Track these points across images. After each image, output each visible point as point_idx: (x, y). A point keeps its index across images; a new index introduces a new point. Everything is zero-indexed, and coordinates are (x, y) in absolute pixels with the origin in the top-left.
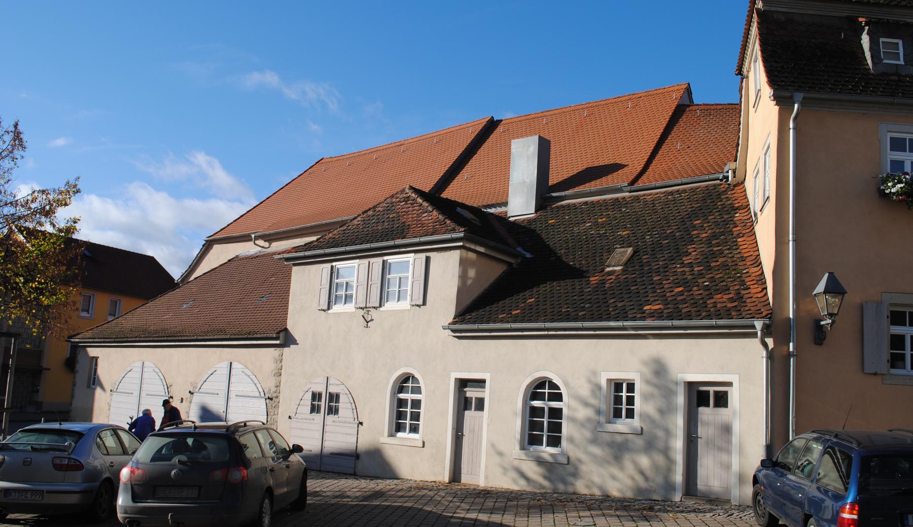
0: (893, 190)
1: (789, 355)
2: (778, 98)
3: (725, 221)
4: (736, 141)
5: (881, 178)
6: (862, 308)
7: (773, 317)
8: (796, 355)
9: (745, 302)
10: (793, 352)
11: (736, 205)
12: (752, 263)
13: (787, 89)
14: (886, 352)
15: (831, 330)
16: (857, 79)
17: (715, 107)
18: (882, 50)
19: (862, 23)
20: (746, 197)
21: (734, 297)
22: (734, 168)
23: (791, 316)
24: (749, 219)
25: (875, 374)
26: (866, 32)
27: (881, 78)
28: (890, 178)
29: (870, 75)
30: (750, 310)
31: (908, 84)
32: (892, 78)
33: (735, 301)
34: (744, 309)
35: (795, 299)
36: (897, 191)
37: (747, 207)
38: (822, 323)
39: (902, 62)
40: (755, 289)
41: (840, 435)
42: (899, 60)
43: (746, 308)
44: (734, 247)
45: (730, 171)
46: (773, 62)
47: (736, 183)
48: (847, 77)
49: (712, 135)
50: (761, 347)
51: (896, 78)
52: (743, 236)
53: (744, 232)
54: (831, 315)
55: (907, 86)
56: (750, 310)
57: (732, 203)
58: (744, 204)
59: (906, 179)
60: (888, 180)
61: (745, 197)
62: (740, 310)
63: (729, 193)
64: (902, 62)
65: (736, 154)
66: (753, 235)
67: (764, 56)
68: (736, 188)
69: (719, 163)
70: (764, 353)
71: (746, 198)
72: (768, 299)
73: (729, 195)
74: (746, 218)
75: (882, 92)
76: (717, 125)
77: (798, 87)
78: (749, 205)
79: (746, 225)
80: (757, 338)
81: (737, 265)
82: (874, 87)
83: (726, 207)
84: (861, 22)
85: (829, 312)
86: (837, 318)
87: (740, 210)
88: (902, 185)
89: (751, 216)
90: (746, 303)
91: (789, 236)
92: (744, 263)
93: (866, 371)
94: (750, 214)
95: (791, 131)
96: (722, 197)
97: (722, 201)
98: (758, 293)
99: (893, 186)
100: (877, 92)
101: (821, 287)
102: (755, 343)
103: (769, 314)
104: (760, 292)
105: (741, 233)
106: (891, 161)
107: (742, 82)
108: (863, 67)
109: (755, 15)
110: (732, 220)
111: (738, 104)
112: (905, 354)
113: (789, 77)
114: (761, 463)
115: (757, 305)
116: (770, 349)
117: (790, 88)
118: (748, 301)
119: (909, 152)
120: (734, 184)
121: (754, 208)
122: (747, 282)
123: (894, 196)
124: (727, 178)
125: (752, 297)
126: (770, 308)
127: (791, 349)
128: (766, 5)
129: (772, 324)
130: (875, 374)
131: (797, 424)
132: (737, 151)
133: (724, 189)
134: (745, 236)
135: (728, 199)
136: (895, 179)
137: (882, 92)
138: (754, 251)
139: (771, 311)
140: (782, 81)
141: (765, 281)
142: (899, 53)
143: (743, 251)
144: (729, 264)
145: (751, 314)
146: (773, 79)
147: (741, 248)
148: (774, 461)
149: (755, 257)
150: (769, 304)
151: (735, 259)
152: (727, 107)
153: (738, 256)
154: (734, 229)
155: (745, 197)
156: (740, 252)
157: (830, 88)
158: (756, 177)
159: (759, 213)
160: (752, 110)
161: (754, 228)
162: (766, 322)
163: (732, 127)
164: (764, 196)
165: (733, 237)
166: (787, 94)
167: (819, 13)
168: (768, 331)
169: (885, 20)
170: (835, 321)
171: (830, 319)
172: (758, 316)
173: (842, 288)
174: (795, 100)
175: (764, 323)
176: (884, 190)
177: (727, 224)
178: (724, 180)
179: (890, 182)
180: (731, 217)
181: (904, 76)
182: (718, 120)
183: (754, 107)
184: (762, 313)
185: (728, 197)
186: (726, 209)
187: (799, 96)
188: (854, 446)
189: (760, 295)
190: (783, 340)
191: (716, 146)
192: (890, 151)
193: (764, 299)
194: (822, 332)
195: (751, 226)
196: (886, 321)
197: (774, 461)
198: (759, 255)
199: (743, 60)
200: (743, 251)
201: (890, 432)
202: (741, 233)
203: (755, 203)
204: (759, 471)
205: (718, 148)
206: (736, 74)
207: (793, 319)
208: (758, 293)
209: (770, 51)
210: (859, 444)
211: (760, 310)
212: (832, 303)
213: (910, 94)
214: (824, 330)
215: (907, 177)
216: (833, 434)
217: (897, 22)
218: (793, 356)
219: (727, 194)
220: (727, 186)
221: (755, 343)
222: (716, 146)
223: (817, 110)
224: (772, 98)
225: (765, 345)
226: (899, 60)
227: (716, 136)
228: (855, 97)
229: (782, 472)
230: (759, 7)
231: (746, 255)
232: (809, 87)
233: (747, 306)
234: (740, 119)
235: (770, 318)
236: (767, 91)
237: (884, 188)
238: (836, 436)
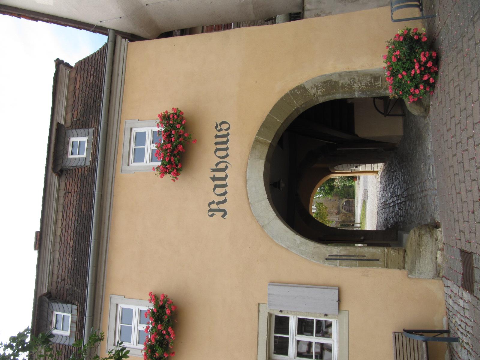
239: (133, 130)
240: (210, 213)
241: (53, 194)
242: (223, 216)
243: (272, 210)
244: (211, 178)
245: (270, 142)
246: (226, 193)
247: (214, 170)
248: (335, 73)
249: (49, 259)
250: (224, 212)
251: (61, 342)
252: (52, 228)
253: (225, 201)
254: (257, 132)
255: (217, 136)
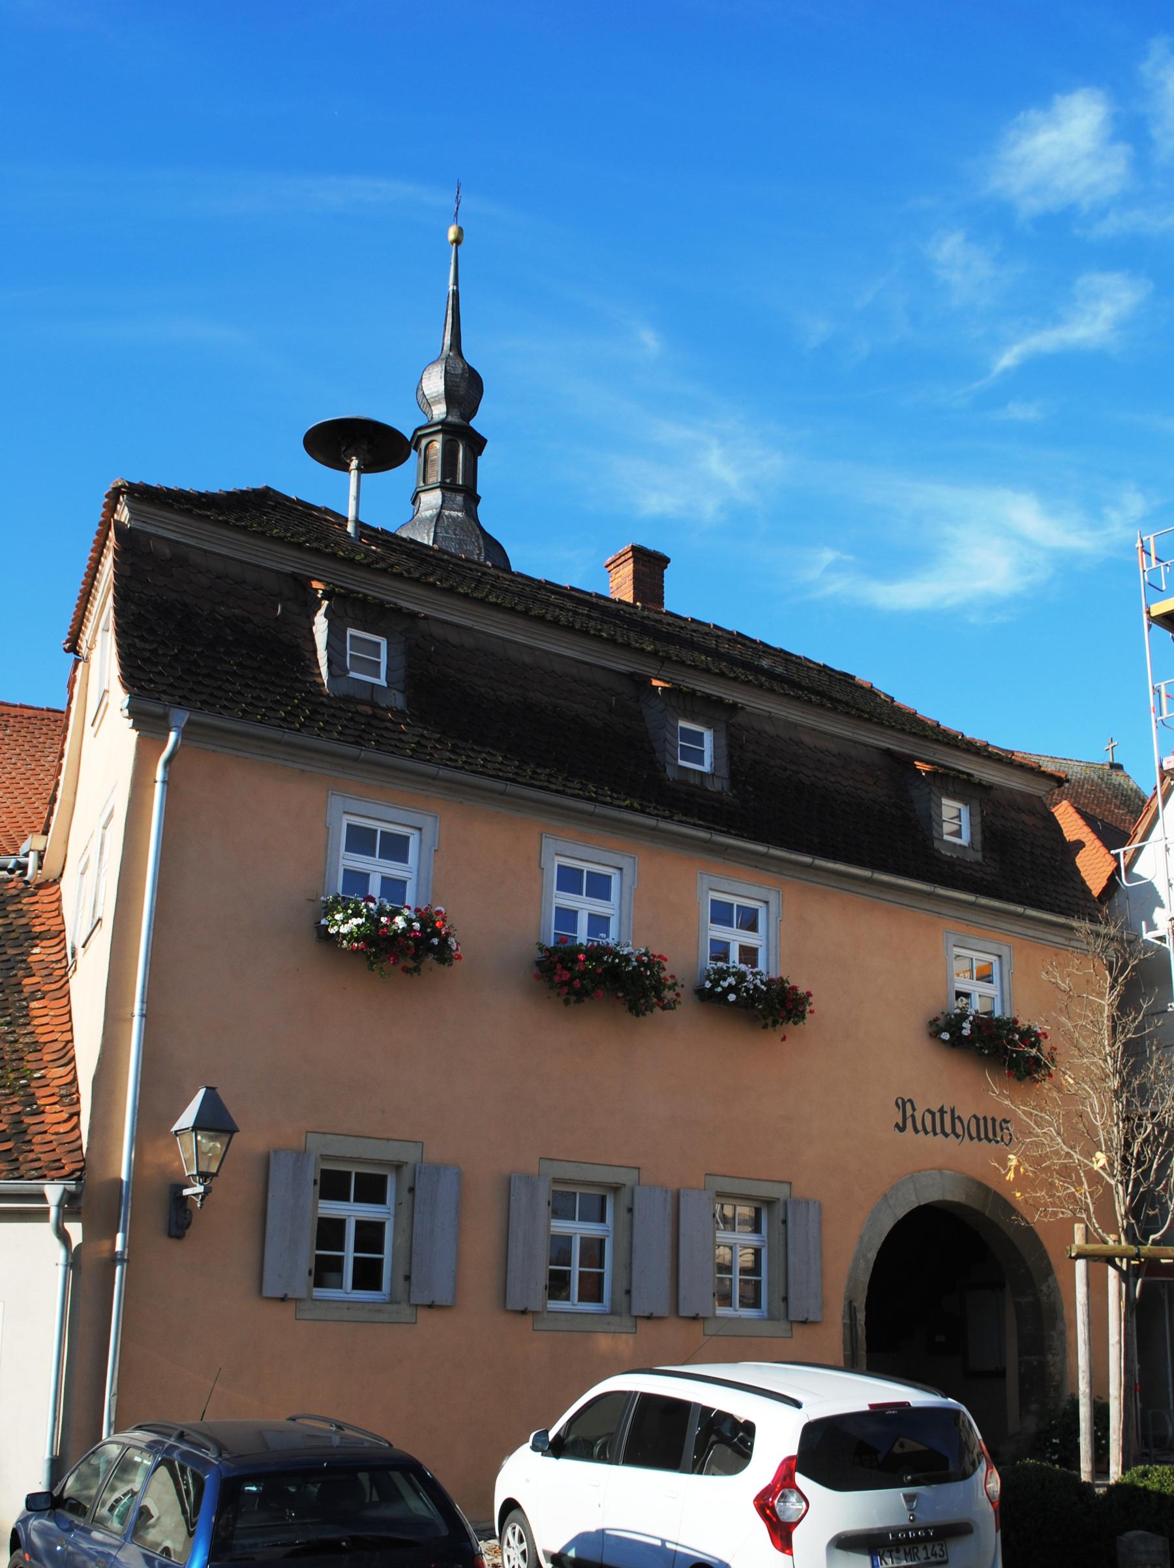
0: (344, 929)
1: (114, 1259)
2: (137, 714)
3: (8, 960)
4: (51, 792)
5: (324, 902)
6: (266, 1163)
7: (85, 1177)
8: (130, 1259)
9: (30, 1141)
10: (122, 1253)
11: (38, 929)
12: (54, 1056)
13: (158, 699)
14: (307, 1253)
15: (201, 1207)
16: (296, 701)
17: (18, 711)
18: (349, 652)
19: (318, 593)
20: (59, 912)
21: (7, 1131)
22: (41, 848)
23: (124, 1176)
24: (59, 961)
25: (283, 1299)
26: (322, 610)
27: (342, 706)
28: (340, 904)
29: (323, 696)
30: (39, 1160)
31: (388, 725)
32: (361, 708)
33: (9, 1140)
34: (26, 1156)
35: (137, 1140)
36: (351, 933)
37: (58, 935)
38: (186, 1192)
39: (382, 681)
40: (54, 1114)
41: (188, 1435)
42: (378, 677)
43: (32, 1156)
44: (22, 1021)
45: (32, 854)
46: (136, 637)
47: (43, 881)
48: (279, 694)
49: (5, 770)
50: (56, 1242)
51: (369, 710)
52: (43, 998)
53: (46, 988)
54: (204, 1176)
55: (386, 729)
56: (39, 1160)
57: (28, 924)
58: (53, 928)
59: (369, 910)
60: (336, 909)
61: (56, 913)
62: (17, 1160)
63: (25, 901)
64: (382, 681)
65: (48, 819)
66: (65, 996)
67: (120, 621)
68: (42, 892)
69: (11, 832)
70: (60, 1254)
71: (60, 915)
72: (80, 1137)
73: (25, 904)
74: (54, 958)
75: (340, 733)
76: (18, 751)
77: (180, 697)
78: (64, 931)
79: (51, 974)
80: (48, 1221)
81: (22, 1059)
82: (327, 721)
83: (14, 931)
84: (316, 590)
85: (200, 1170)
86: (215, 1183)
87: (42, 940)
88: (360, 921)
89: (66, 956)
90: (33, 1144)
91: (133, 1006)
92: (37, 1055)
93: (267, 1292)
94: (63, 952)
95: (158, 788)
96: (9, 908)
97: (7, 916)
98: (59, 1123)
99: (345, 921)
100: (332, 731)
101: (188, 1118)
102: (44, 1231)
103: (77, 1170)
104: (65, 1121)
105: (39, 990)
106: (345, 870)
107: (75, 668)
108: (311, 679)
109: (112, 534)
110: (25, 961)
111: (62, 712)
112: (342, 1257)
113: (166, 674)
114: (27, 1501)
115: (54, 1150)
116: (74, 1246)
117: (164, 697)
118: (38, 1139)
119: (380, 857)
120: (36, 882)
121: (74, 937)
122: (39, 1098)
123: (345, 942)
124: (24, 867)
125: (45, 1132)
126: (81, 1158)
127: (119, 1247)
128: (135, 517)
129: (82, 1191)
130: (283, 1299)
131: (119, 1409)
132: (51, 813)
133: (14, 892)
134: (46, 997)
135: (21, 913)
136: (349, 908)
137: (340, 733)
138: (63, 1032)
139: (82, 1164)
140: (151, 681)
141: (78, 1099)
142: (379, 663)
143: (40, 1030)
144: (6, 1057)
145: (40, 1168)
146: (132, 676)
147: (36, 1022)
148: (55, 1495)
149: (64, 1043)
150: (81, 1147)
151: (21, 1046)
152: (45, 714)
153: (27, 1040)
154: (26, 981)
155: (56, 913)
156: (33, 1032)
157: (244, 711)
158: (83, 874)
159: (80, 951)
160: (89, 731)
161: (67, 981)
162: (68, 1187)
163: (50, 759)
164: (93, 917)
165: (22, 998)
166: (158, 709)
167: (238, 555)
168: (71, 1206)
169: (361, 595)
170: (211, 1188)
171: (201, 1184)
172: (53, 1173)
173: (232, 1122)
174: (173, 724)
175: (65, 1190)
176: (327, 927)
177: (13, 968)
178: (18, 872)
179: (339, 912)
180: (22, 954)
181: (383, 709)
182: (21, 740)
183: (92, 725)
184: (63, 1168)
185: (21, 909)
186: (13, 935)
187: (181, 717)
188: (211, 1456)
189: (63, 1128)
190: (100, 1229)
191: (11, 795)
192: (346, 851)
193: (72, 1136)
194: (186, 1210)
195: (63, 976)
196: (311, 1190)
197: (55, 1495)
198: (72, 1041)
199: (82, 623)
200: (40, 1030)
201: (291, 1422)
202: (39, 990)
203: (75, 928)
204: (24, 1521)
205: (15, 801)
206: (64, 649)
207: (128, 1183)
208: (59, 1123)
209: (133, 614)
210: (221, 1449)
211: (60, 1160)
212: (208, 1152)
213: (391, 745)
214: (188, 1207)
215: (371, 905)
216: (176, 1433)
217: (381, 604)
218: (122, 1261)
219: (20, 902)
220: (22, 885)
221: (44, 1231)
222: (11, 795)
223: (213, 751)
224: (126, 712)
225: (64, 1237)
226: (378, 677)
227: (13, 774)
228: (289, 737)
229: (71, 1522)
230: (123, 520)
231: (43, 1039)
232: (203, 702)
233: (32, 1151)
234: (63, 745)
235: (79, 1179)
236: (119, 698)
237: (327, 923)
238: (181, 1437)
239: (416, 833)
240: (900, 1101)
241: (865, 734)
242: (897, 1125)
243: (906, 1213)
244: (942, 1107)
245: (987, 1213)
246: (926, 1133)
247: (953, 1111)
248: (1064, 1324)
249: (761, 707)
250: (901, 1128)
251: (947, 807)
252: (812, 722)
253: (917, 1131)
254: (999, 1192)
255: (994, 1120)
